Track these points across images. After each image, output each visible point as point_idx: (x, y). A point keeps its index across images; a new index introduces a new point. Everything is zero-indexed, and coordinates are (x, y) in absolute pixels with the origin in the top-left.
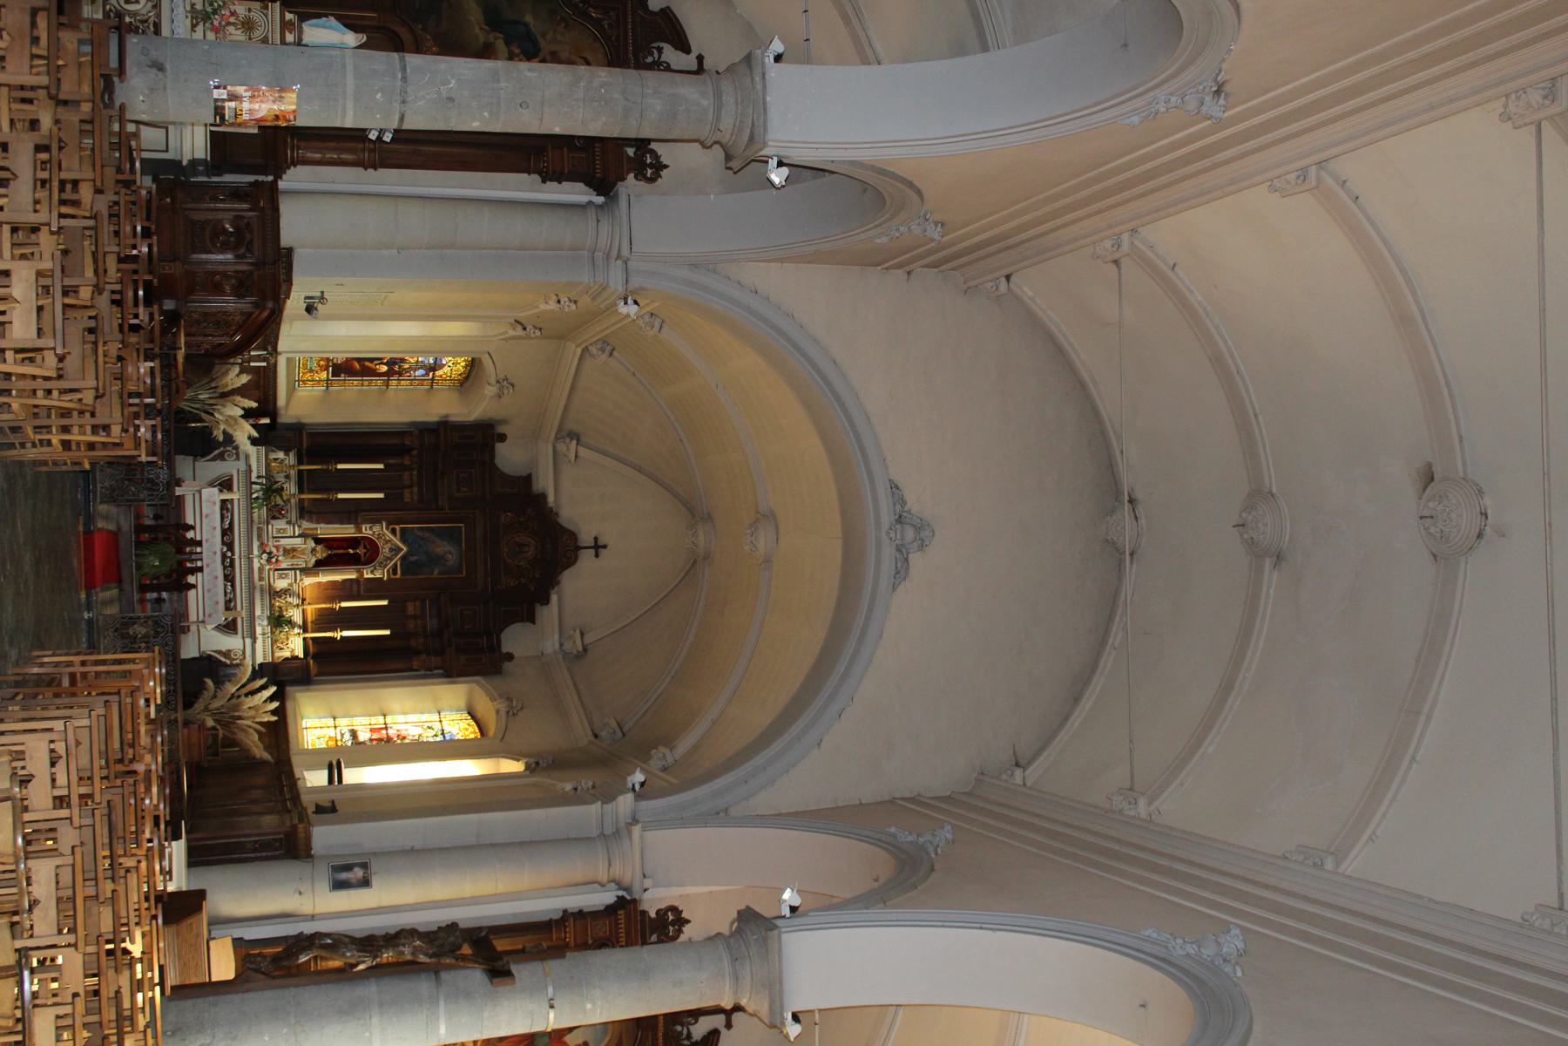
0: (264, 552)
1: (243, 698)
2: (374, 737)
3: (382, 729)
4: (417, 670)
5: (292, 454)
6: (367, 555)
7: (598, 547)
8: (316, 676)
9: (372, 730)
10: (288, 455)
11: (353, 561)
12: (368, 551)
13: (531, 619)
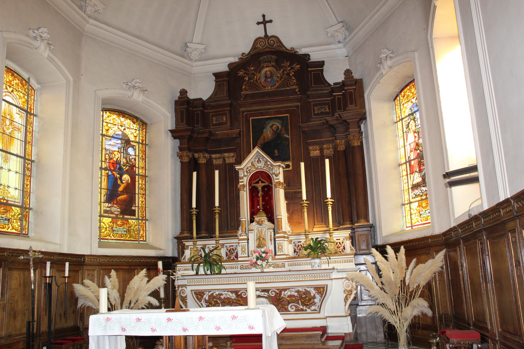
0: (256, 263)
1: (383, 279)
2: (418, 170)
3: (410, 165)
4: (362, 143)
5: (187, 244)
6: (264, 181)
7: (264, 22)
8: (368, 221)
9: (412, 173)
10: (188, 246)
11: (268, 192)
12: (260, 180)
13: (321, 64)
